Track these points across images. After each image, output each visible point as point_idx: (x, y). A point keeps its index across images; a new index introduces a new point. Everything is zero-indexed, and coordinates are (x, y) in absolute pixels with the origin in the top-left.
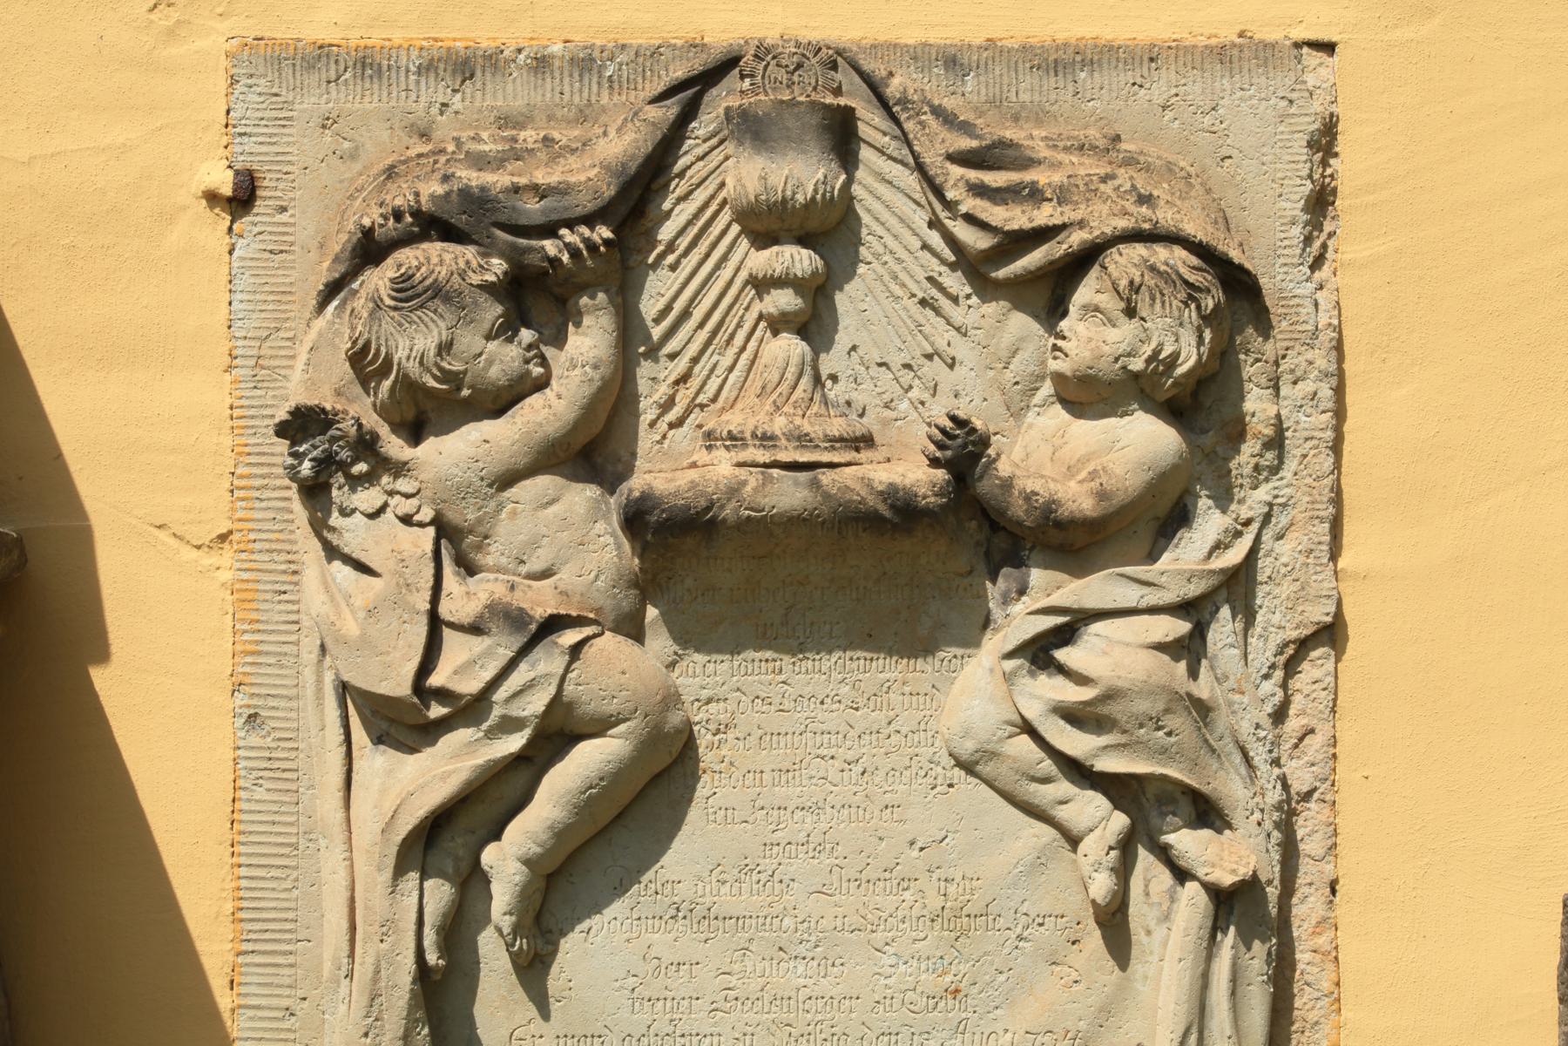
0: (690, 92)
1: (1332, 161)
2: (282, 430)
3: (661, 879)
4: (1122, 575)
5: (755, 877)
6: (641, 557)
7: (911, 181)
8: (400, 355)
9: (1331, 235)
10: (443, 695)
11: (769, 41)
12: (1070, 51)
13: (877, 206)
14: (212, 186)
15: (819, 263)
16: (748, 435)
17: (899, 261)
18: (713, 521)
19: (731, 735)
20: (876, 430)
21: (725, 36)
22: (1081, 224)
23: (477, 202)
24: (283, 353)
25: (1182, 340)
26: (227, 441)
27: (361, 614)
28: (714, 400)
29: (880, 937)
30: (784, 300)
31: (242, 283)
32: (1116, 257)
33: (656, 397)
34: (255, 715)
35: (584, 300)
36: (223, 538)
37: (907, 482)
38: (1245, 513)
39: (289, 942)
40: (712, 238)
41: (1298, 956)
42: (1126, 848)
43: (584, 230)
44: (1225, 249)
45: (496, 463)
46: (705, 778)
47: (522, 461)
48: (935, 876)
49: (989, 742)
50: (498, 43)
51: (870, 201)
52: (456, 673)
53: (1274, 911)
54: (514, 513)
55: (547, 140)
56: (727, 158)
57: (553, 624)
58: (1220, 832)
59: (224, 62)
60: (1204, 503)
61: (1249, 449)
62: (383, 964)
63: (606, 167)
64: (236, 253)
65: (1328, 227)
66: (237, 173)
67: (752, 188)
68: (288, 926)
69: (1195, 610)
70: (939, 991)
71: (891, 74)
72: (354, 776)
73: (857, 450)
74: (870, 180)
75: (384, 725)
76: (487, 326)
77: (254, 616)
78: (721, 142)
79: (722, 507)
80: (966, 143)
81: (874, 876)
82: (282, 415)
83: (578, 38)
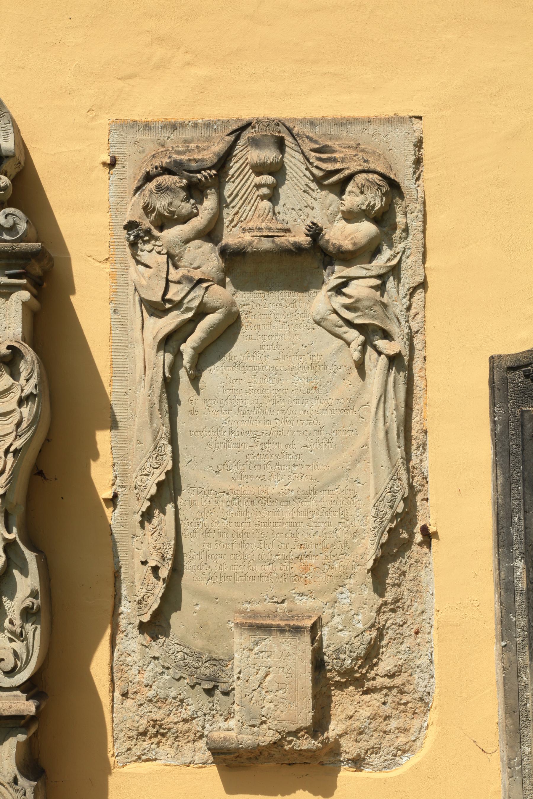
0: (238, 133)
1: (421, 150)
2: (125, 227)
3: (231, 355)
4: (361, 267)
5: (258, 355)
6: (225, 263)
7: (300, 157)
8: (158, 206)
9: (422, 171)
10: (170, 301)
11: (260, 118)
12: (345, 120)
13: (291, 164)
14: (104, 161)
15: (274, 180)
16: (255, 228)
17: (297, 179)
18: (245, 252)
19: (250, 315)
20: (291, 227)
21: (247, 117)
22: (348, 168)
23: (179, 164)
24: (124, 207)
25: (377, 200)
26: (108, 232)
27: (147, 279)
28: (245, 219)
29: (294, 372)
30: (264, 191)
31: (112, 188)
32: (358, 177)
33: (228, 219)
34: (116, 309)
35: (208, 191)
36: (107, 259)
37: (299, 241)
38: (397, 250)
39: (126, 373)
40: (244, 174)
41: (415, 378)
42: (364, 346)
43: (208, 171)
44: (389, 175)
45: (184, 237)
46: (243, 327)
47: (191, 236)
48: (309, 355)
49: (324, 316)
50: (183, 120)
51: (289, 163)
52: (173, 295)
53: (407, 364)
54: (189, 250)
55: (198, 147)
56: (248, 151)
57: (201, 281)
58: (391, 341)
59: (108, 126)
60: (385, 247)
61: (398, 232)
62: (154, 375)
63: (215, 154)
64: (111, 179)
65: (421, 169)
66: (111, 157)
67: (255, 159)
68: (126, 369)
69: (383, 277)
70: (311, 388)
71: (294, 127)
72: (144, 326)
73: (286, 232)
74: (289, 157)
75: (153, 311)
76: (181, 198)
77: (116, 281)
78: (247, 147)
79: (247, 248)
80: (316, 146)
81: (292, 355)
82: (125, 223)
83: (206, 118)
